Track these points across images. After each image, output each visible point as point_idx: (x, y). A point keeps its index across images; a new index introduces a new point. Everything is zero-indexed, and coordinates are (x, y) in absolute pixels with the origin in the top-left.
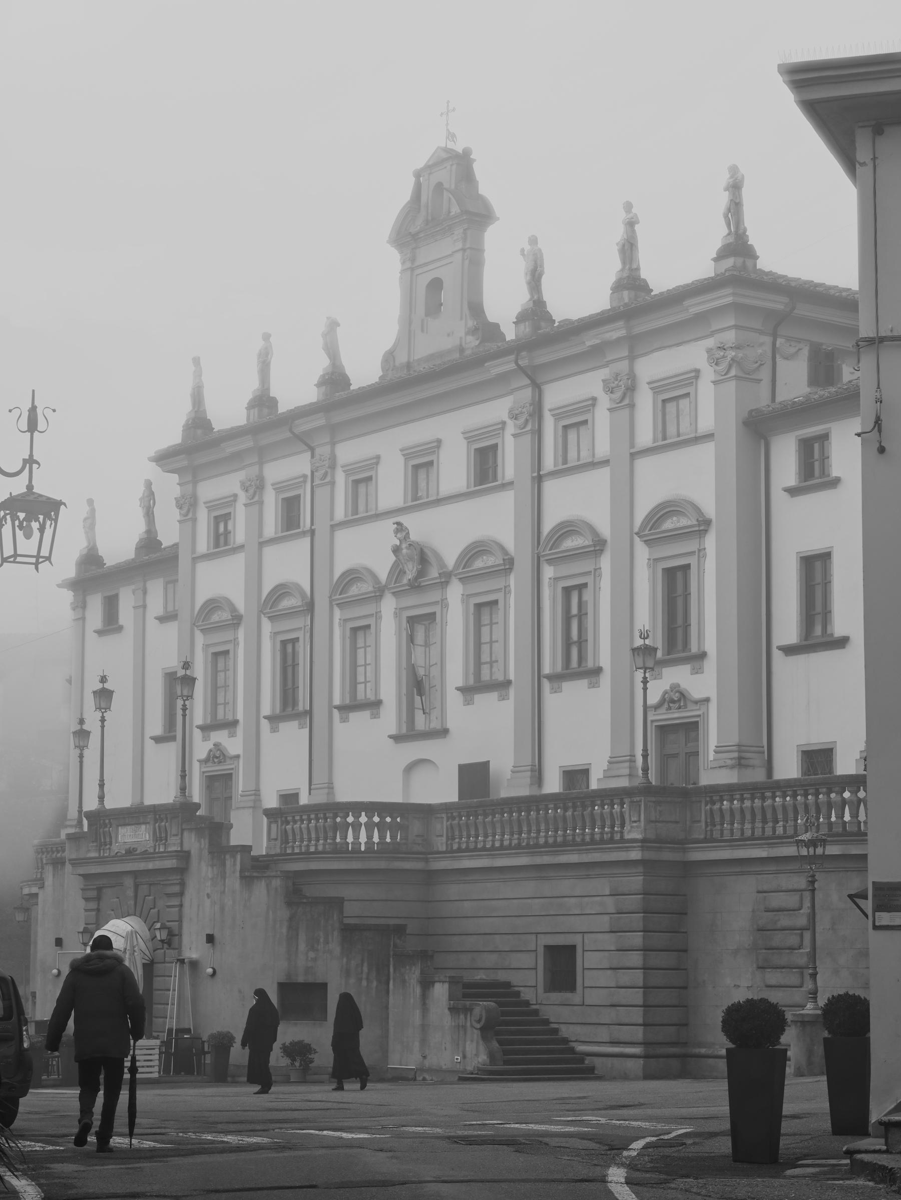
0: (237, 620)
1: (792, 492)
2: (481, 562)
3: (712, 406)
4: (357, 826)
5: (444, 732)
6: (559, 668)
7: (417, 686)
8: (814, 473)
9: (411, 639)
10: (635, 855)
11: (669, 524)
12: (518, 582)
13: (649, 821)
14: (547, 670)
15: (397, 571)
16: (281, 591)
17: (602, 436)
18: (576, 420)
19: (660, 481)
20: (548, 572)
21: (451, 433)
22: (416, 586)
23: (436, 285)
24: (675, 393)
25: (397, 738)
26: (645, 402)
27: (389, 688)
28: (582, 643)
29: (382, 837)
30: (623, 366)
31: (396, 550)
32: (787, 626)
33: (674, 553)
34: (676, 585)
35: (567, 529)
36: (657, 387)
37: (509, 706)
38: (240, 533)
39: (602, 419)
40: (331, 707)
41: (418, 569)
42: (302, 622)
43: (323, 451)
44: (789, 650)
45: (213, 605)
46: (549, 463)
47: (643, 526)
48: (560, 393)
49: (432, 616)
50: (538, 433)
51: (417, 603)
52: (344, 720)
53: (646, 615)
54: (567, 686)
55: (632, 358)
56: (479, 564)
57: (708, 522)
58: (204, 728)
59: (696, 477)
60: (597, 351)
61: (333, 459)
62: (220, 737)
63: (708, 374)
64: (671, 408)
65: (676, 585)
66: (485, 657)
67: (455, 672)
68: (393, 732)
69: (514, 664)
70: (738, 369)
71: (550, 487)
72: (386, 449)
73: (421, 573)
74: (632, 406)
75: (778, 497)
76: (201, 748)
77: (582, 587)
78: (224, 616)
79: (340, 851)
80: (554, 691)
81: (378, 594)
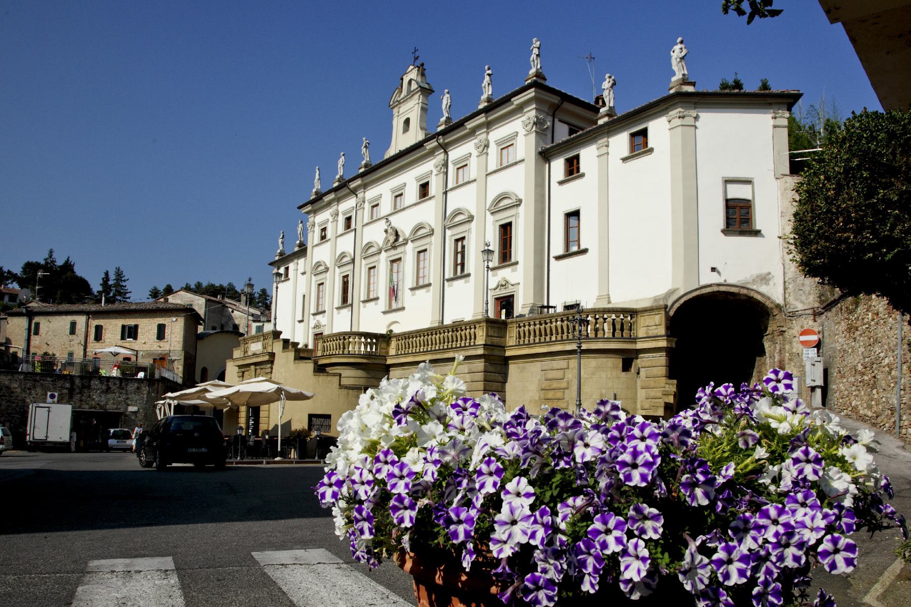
0: (327, 269)
1: (561, 183)
2: (420, 232)
3: (526, 145)
4: (360, 343)
5: (403, 308)
6: (452, 276)
7: (393, 292)
8: (573, 169)
9: (391, 270)
10: (480, 351)
11: (503, 203)
12: (436, 239)
13: (487, 336)
14: (447, 277)
15: (387, 241)
16: (343, 255)
17: (473, 171)
18: (462, 166)
19: (497, 185)
20: (448, 233)
21: (409, 179)
22: (394, 247)
23: (407, 122)
24: (506, 145)
25: (384, 313)
26: (493, 150)
27: (382, 291)
28: (463, 265)
29: (371, 348)
30: (484, 136)
31: (386, 231)
32: (558, 248)
33: (504, 218)
34: (506, 230)
35: (458, 212)
36: (498, 143)
37: (431, 294)
38: (329, 236)
39: (473, 162)
40: (360, 301)
41: (396, 239)
42: (351, 266)
43: (360, 195)
44: (558, 258)
45: (318, 264)
46: (450, 186)
47: (490, 207)
48: (455, 154)
49: (400, 259)
50: (446, 173)
51: (394, 254)
52: (364, 307)
53: (493, 238)
54: (455, 283)
55: (488, 133)
56: (420, 233)
57: (521, 201)
58: (314, 315)
59: (518, 181)
60: (473, 132)
61: (364, 198)
62: (319, 317)
63: (522, 132)
64: (505, 151)
65: (506, 230)
66: (421, 275)
67: (409, 280)
68: (383, 310)
69: (433, 275)
70: (541, 129)
71: (449, 195)
72: (383, 190)
73: (396, 240)
74: (487, 154)
75: (554, 184)
76: (312, 324)
77: (463, 238)
78: (322, 268)
79: (350, 355)
80: (449, 286)
81: (379, 253)
